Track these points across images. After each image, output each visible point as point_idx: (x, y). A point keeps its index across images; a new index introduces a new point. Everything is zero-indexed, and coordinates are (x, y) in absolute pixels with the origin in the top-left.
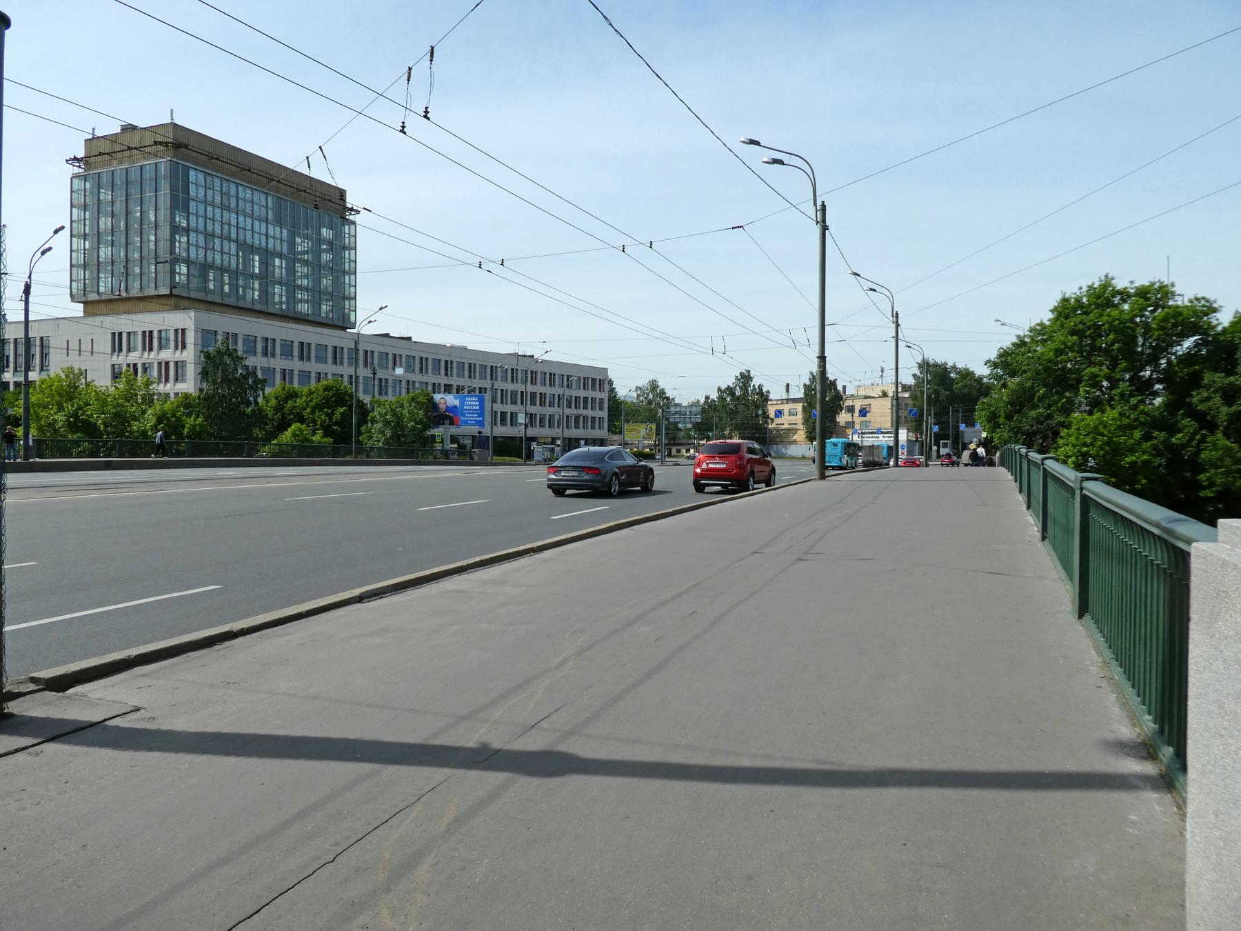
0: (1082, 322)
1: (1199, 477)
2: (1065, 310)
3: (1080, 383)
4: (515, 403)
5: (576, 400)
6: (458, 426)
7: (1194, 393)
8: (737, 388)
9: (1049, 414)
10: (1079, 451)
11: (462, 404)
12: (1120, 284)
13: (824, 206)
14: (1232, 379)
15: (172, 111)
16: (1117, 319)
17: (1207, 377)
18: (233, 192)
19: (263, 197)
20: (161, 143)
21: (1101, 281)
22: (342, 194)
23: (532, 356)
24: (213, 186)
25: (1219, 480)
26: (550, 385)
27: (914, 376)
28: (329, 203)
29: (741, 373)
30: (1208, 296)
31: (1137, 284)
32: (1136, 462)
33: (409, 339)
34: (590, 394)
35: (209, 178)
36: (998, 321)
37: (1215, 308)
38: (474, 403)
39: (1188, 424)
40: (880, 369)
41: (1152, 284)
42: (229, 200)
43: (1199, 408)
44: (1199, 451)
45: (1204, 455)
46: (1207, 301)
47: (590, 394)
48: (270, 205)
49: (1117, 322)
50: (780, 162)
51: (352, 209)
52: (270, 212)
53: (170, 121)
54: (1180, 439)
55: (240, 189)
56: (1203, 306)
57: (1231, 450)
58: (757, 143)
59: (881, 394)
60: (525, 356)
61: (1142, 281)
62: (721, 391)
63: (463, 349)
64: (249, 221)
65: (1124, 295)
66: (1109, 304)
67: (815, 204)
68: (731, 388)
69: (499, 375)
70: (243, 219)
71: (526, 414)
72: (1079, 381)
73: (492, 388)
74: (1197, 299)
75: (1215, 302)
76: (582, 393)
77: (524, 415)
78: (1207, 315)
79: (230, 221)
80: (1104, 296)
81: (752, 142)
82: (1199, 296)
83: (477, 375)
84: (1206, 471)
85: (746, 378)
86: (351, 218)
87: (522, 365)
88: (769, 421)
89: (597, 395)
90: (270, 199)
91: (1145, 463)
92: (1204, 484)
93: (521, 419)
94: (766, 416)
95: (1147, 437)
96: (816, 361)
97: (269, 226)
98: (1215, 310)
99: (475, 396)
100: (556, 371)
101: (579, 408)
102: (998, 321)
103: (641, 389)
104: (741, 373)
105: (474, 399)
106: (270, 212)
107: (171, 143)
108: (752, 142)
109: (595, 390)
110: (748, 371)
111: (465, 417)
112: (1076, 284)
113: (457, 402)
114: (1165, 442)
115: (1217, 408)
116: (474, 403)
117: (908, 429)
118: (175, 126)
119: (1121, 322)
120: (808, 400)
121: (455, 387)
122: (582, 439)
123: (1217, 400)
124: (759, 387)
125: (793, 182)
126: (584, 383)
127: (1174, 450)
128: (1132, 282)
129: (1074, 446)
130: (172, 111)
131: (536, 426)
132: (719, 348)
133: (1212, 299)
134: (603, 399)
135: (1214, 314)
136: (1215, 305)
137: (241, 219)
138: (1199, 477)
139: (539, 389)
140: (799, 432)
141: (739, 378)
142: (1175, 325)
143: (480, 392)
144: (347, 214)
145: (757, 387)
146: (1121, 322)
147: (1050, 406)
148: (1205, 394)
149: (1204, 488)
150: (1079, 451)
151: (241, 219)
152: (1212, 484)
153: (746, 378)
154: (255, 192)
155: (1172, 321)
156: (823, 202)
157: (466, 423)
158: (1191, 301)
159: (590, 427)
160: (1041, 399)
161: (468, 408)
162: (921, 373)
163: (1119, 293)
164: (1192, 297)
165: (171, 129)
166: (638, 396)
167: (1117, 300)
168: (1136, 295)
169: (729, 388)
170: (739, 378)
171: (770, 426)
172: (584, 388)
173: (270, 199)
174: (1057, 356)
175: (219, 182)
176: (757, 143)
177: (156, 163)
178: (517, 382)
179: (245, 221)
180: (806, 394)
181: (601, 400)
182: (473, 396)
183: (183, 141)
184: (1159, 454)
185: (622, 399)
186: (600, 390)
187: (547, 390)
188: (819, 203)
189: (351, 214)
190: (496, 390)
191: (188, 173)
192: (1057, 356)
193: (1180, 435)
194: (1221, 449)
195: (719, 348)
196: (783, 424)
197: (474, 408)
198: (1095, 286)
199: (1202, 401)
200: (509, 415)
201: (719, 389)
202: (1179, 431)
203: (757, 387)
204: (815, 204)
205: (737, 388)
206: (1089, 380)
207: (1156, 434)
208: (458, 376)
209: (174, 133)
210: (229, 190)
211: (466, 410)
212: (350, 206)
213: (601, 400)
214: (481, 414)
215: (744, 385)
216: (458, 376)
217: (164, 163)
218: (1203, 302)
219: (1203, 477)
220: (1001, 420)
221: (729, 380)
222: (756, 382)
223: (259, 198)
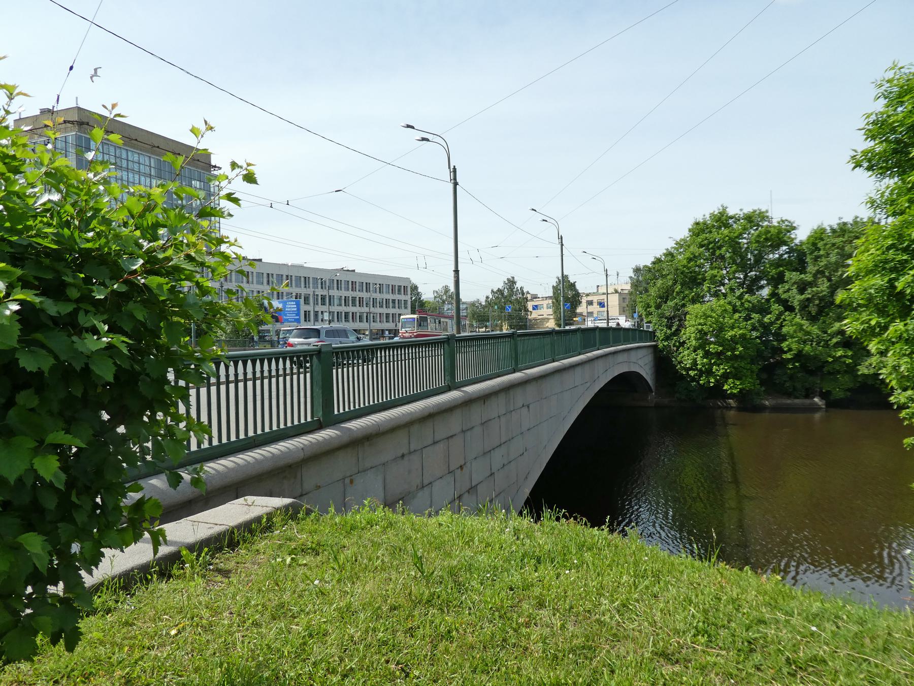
0: (706, 239)
1: (782, 345)
2: (699, 229)
3: (705, 281)
4: (340, 305)
5: (386, 302)
6: (282, 323)
7: (780, 286)
8: (506, 290)
9: (684, 304)
10: (697, 329)
11: (284, 307)
12: (731, 212)
13: (455, 169)
14: (803, 276)
15: (77, 98)
16: (727, 236)
17: (787, 275)
18: (124, 156)
19: (147, 159)
20: (69, 122)
21: (719, 209)
22: (208, 156)
23: (354, 271)
24: (109, 151)
25: (794, 346)
26: (367, 291)
27: (631, 277)
28: (199, 163)
29: (508, 279)
30: (789, 219)
31: (745, 211)
32: (735, 336)
33: (260, 260)
34: (397, 297)
35: (105, 147)
36: (670, 238)
37: (795, 227)
38: (293, 306)
39: (776, 308)
40: (616, 273)
41: (755, 211)
42: (122, 162)
43: (782, 297)
44: (782, 326)
45: (784, 330)
46: (790, 222)
47: (397, 297)
48: (153, 165)
49: (727, 238)
50: (427, 140)
51: (215, 167)
52: (153, 170)
53: (75, 106)
54: (769, 319)
55: (130, 154)
56: (787, 226)
57: (802, 325)
58: (413, 127)
59: (614, 291)
60: (348, 270)
61: (748, 209)
62: (494, 292)
63: (302, 267)
64: (137, 177)
65: (736, 219)
66: (727, 226)
67: (449, 168)
68: (501, 290)
69: (343, 286)
70: (132, 175)
71: (330, 312)
72: (704, 280)
73: (314, 295)
74: (783, 221)
75: (794, 223)
76: (391, 297)
77: (328, 314)
78: (789, 231)
79: (122, 177)
80: (722, 220)
81: (408, 126)
82: (784, 219)
83: (311, 285)
84: (786, 340)
85: (511, 282)
86: (215, 173)
87: (343, 277)
88: (529, 313)
89: (402, 297)
90: (152, 160)
91: (743, 336)
92: (785, 349)
93: (326, 316)
94: (526, 310)
95: (748, 318)
96: (452, 274)
97: (152, 180)
98: (794, 228)
99: (294, 301)
100: (371, 281)
101: (348, 305)
102: (670, 238)
103: (437, 292)
104: (508, 279)
105: (293, 303)
106: (153, 170)
107: (76, 121)
108: (408, 126)
109: (401, 294)
110: (513, 278)
111: (286, 316)
112: (704, 211)
113: (280, 306)
114: (759, 321)
115: (794, 297)
116: (293, 306)
117: (626, 316)
118: (79, 109)
119: (730, 238)
120: (556, 297)
121: (294, 294)
122: (387, 330)
123: (795, 290)
124: (521, 288)
125: (434, 151)
126: (392, 289)
127: (766, 328)
128: (741, 210)
129: (693, 326)
130: (77, 98)
131: (356, 322)
132: (422, 265)
133: (792, 221)
134: (407, 301)
135: (794, 231)
136: (794, 225)
137: (131, 175)
138: (782, 345)
139: (358, 294)
140: (550, 320)
141: (507, 282)
142: (767, 239)
143: (296, 298)
144: (212, 169)
145: (519, 289)
146: (730, 238)
147: (683, 299)
148: (787, 287)
149: (786, 352)
150: (697, 329)
151: (131, 175)
152: (790, 350)
153: (511, 282)
154: (141, 156)
155: (764, 237)
156: (454, 166)
157: (287, 320)
158: (779, 223)
159: (385, 321)
160: (678, 293)
161: (289, 310)
162: (635, 275)
163: (731, 218)
164: (779, 220)
165: (76, 111)
166: (435, 297)
167: (731, 221)
168: (744, 219)
169: (499, 290)
170: (507, 282)
171: (529, 317)
172: (392, 293)
173: (152, 160)
174: (689, 262)
175: (113, 149)
176: (413, 127)
177: (65, 137)
178: (341, 290)
179: (134, 177)
180: (554, 293)
181: (406, 301)
182: (292, 301)
183: (85, 120)
184: (754, 328)
185: (425, 300)
186: (404, 294)
187: (364, 295)
188: (452, 167)
189: (215, 170)
190: (317, 295)
191: (90, 144)
192: (689, 262)
193: (769, 316)
194: (795, 325)
195: (422, 265)
196: (543, 315)
197: (293, 309)
198: (716, 213)
199: (785, 292)
200: (351, 314)
201: (492, 291)
202: (770, 313)
203: (519, 289)
204: (449, 168)
205: (506, 290)
206: (710, 279)
207: (753, 315)
208: (296, 286)
209: (78, 114)
210: (121, 154)
211: (287, 311)
212: (214, 165)
213: (406, 301)
214: (298, 314)
215: (510, 288)
216: (296, 286)
217: (71, 134)
218: (787, 223)
219: (784, 345)
220: (652, 309)
221: (499, 285)
222: (518, 285)
223: (144, 160)
